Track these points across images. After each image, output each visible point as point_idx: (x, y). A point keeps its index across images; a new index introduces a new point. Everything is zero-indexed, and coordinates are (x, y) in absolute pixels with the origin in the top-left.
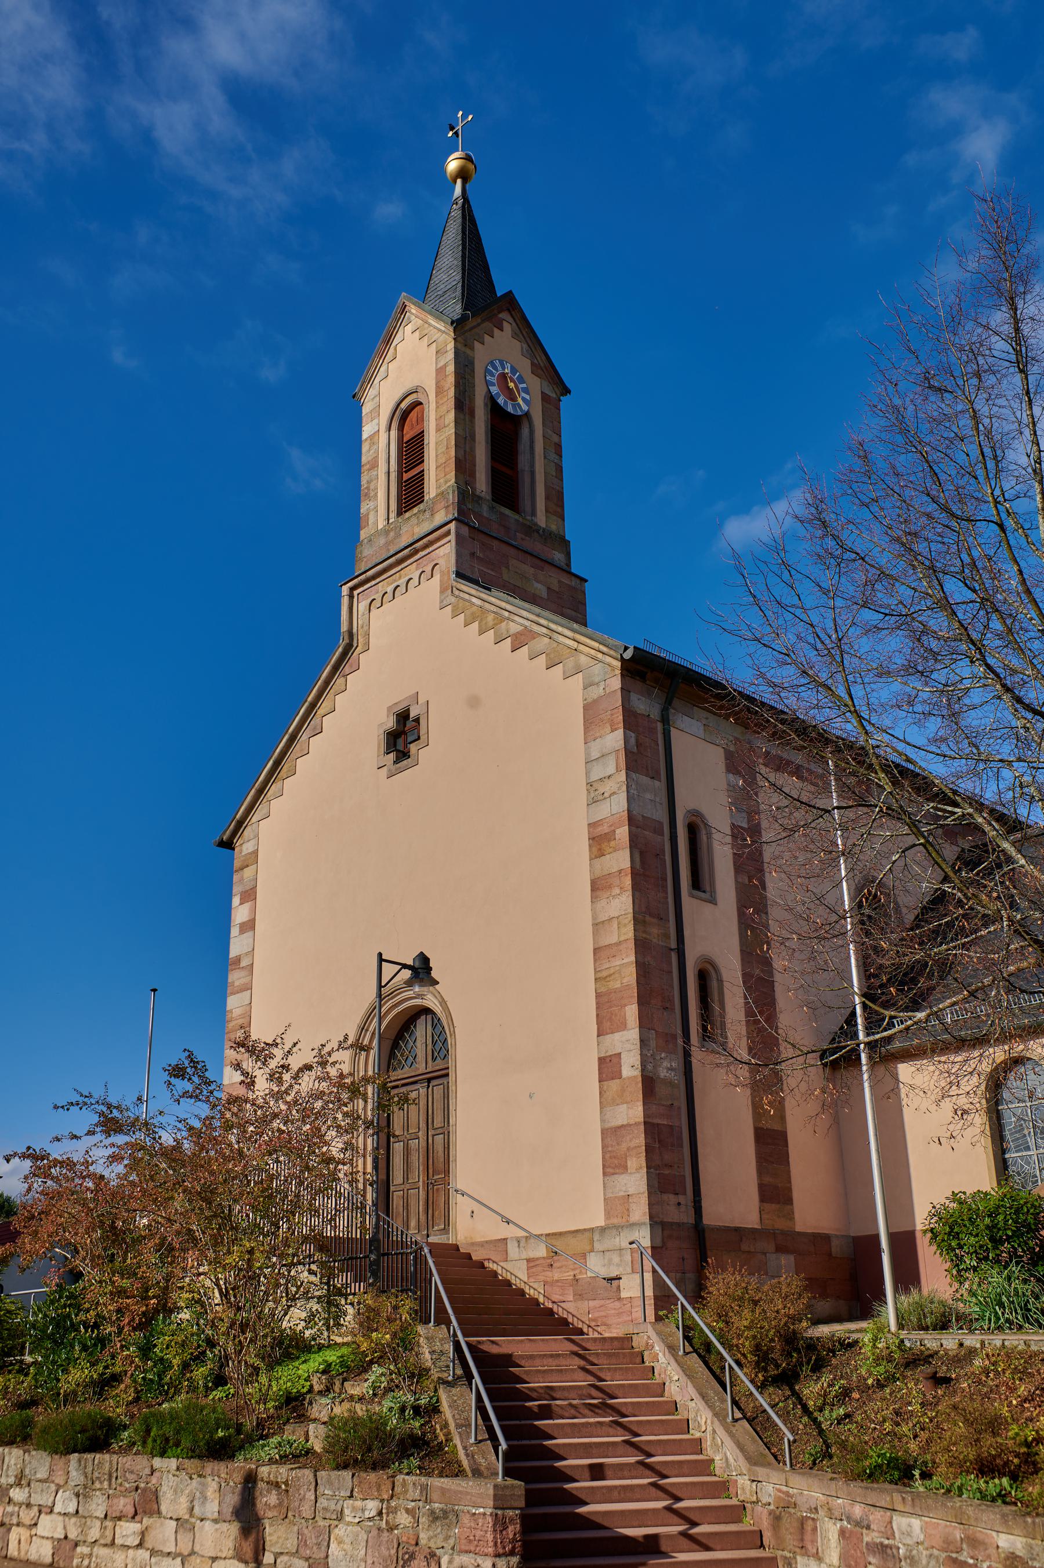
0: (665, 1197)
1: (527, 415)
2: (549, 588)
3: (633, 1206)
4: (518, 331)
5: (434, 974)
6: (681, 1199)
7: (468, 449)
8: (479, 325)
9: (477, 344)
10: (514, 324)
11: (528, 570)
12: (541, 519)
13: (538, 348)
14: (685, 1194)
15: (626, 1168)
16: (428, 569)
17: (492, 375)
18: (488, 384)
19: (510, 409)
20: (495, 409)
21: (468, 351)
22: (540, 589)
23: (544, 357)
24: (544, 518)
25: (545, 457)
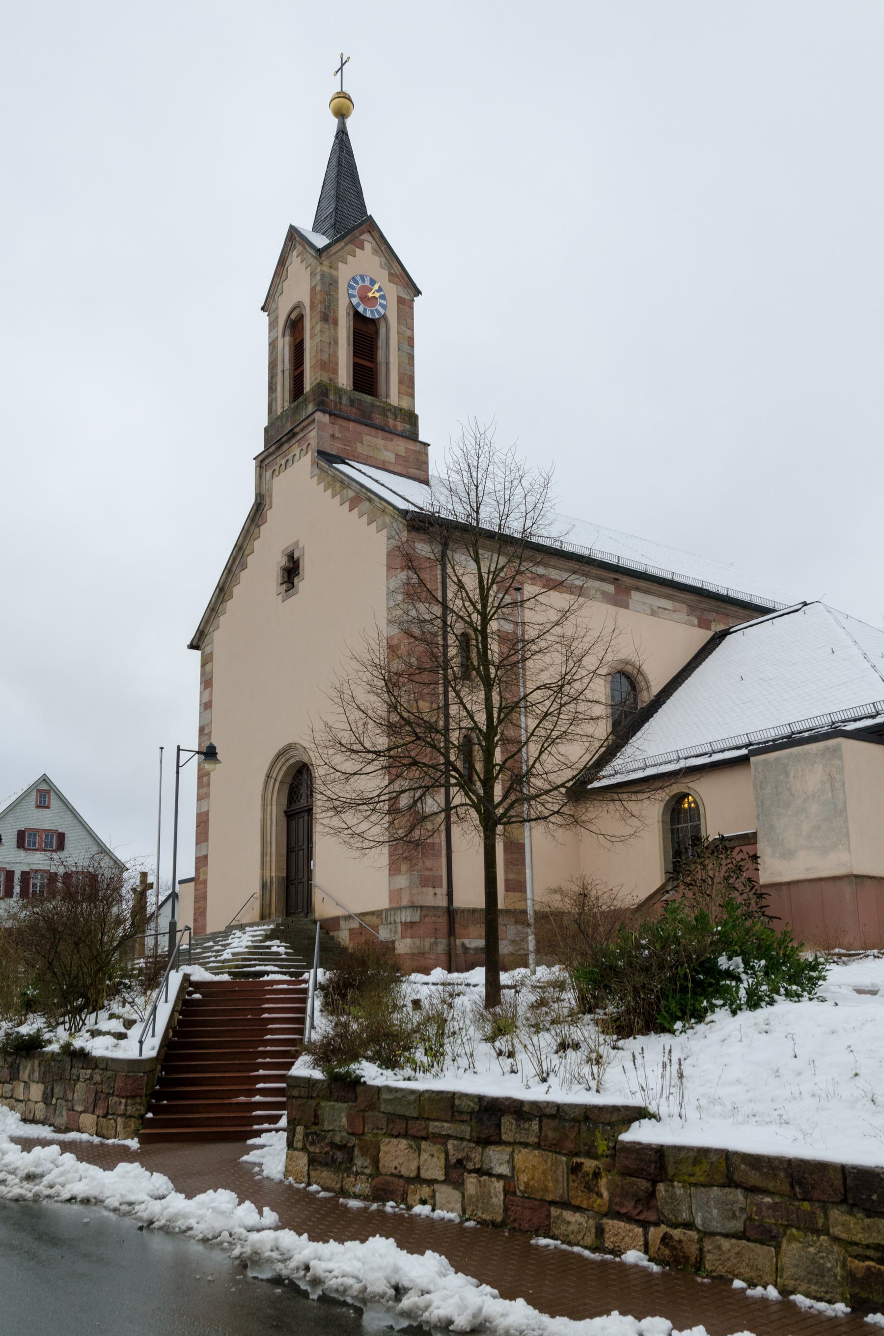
0: (425, 889)
1: (384, 317)
2: (396, 455)
3: (403, 896)
4: (378, 249)
5: (218, 756)
6: (438, 891)
7: (332, 351)
8: (342, 248)
9: (340, 264)
10: (374, 243)
11: (380, 442)
12: (394, 399)
13: (395, 260)
14: (441, 887)
15: (400, 871)
16: (305, 447)
17: (354, 288)
18: (350, 296)
19: (368, 315)
20: (358, 317)
21: (333, 272)
22: (389, 457)
23: (399, 267)
24: (397, 399)
25: (399, 350)
